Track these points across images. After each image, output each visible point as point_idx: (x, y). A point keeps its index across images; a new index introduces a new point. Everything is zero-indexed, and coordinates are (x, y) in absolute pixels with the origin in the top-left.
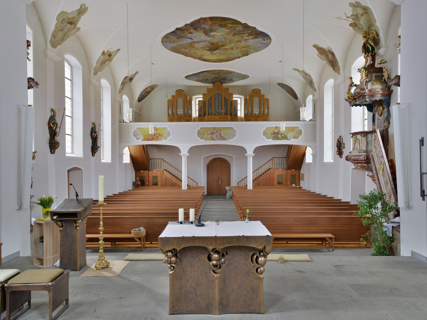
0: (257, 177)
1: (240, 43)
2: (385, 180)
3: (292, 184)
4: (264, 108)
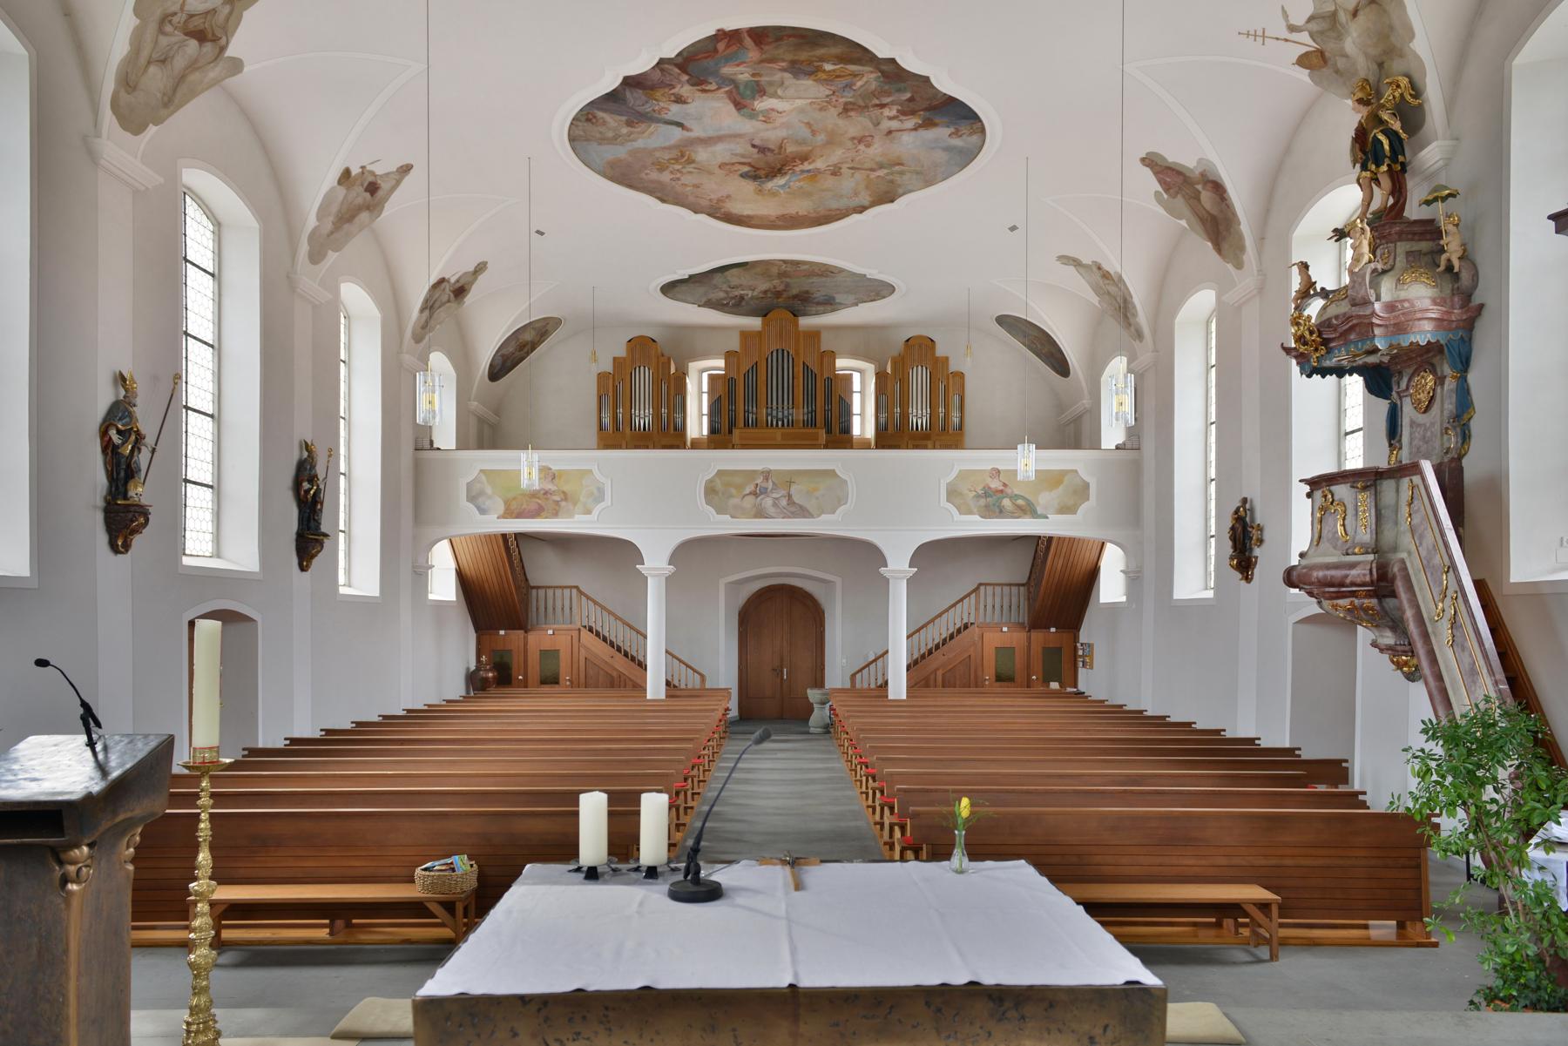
0: (923, 657)
1: (868, 146)
2: (1467, 660)
3: (1046, 681)
4: (946, 406)
